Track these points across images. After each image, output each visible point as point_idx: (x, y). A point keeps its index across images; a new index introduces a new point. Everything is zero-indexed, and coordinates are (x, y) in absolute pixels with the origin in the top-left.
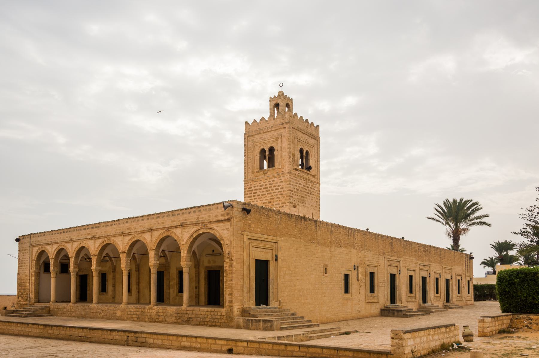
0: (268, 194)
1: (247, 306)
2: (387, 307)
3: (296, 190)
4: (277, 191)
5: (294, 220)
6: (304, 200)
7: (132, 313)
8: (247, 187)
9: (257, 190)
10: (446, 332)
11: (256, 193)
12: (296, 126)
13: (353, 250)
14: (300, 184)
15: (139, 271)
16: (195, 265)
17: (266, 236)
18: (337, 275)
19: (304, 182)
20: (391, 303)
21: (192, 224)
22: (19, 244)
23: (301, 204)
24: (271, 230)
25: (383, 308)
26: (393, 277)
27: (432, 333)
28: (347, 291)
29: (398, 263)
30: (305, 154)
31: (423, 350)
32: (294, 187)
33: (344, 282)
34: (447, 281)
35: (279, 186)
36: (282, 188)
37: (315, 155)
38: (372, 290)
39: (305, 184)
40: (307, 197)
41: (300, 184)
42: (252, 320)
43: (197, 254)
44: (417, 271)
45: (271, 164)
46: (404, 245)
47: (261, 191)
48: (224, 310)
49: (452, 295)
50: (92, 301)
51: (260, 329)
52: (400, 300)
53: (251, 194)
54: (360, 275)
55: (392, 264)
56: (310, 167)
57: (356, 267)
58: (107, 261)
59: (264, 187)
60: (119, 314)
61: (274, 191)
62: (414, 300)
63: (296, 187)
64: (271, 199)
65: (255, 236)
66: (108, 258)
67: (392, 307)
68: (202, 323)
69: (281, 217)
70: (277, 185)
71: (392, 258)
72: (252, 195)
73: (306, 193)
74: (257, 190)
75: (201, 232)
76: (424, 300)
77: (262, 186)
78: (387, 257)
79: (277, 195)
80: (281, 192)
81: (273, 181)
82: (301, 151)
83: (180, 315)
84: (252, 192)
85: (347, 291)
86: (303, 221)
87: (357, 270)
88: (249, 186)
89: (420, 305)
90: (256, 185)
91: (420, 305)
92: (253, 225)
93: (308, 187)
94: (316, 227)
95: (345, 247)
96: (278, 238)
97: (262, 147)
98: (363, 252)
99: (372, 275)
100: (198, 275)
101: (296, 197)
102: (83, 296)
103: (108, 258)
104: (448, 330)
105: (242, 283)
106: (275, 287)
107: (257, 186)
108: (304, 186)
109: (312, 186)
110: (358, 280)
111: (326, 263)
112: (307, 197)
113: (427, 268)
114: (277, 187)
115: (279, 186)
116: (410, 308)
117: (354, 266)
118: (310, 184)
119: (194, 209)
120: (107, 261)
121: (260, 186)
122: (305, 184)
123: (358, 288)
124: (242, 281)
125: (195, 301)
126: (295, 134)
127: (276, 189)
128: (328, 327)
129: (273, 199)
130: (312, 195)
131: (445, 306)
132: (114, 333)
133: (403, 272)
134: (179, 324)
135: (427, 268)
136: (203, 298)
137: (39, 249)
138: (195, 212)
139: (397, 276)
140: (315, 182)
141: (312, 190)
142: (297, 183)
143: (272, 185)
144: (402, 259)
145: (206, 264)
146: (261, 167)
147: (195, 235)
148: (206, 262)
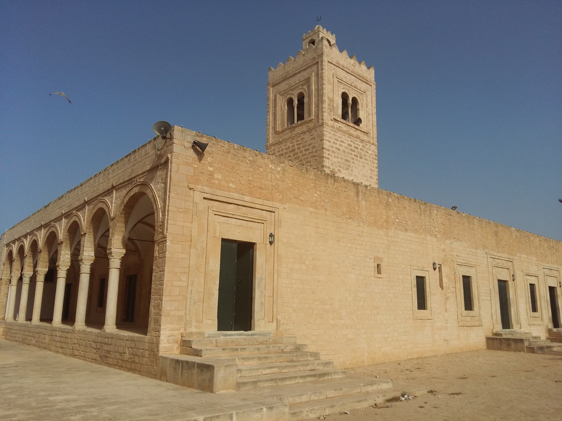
1: (193, 330)
2: (496, 334)
4: (307, 152)
6: (349, 166)
12: (335, 60)
13: (429, 238)
14: (342, 142)
17: (247, 198)
18: (401, 277)
19: (349, 139)
20: (504, 328)
24: (261, 188)
25: (490, 335)
26: (503, 286)
28: (422, 304)
29: (510, 264)
32: (331, 144)
33: (415, 289)
35: (309, 145)
36: (315, 147)
37: (367, 105)
38: (469, 305)
39: (352, 143)
41: (342, 142)
46: (516, 236)
47: (287, 156)
48: (147, 338)
52: (519, 322)
54: (444, 280)
55: (500, 265)
57: (437, 266)
59: (291, 149)
61: (304, 153)
62: (539, 322)
65: (221, 194)
67: (506, 334)
69: (284, 170)
70: (307, 144)
71: (499, 254)
73: (353, 156)
77: (289, 148)
78: (492, 253)
79: (307, 158)
80: (312, 152)
81: (302, 139)
82: (345, 96)
85: (422, 304)
86: (330, 181)
87: (440, 271)
90: (281, 149)
92: (217, 176)
93: (356, 148)
95: (416, 231)
96: (277, 205)
97: (288, 97)
98: (448, 242)
99: (467, 280)
101: (336, 160)
105: (185, 284)
107: (282, 150)
108: (349, 145)
109: (363, 146)
110: (441, 286)
111: (379, 256)
112: (355, 161)
113: (555, 273)
114: (307, 147)
115: (309, 145)
116: (535, 334)
117: (434, 264)
121: (286, 149)
122: (352, 143)
123: (445, 300)
126: (333, 72)
127: (305, 150)
130: (363, 160)
133: (518, 279)
137: (48, 230)
139: (510, 283)
140: (369, 142)
141: (363, 153)
142: (337, 140)
144: (515, 258)
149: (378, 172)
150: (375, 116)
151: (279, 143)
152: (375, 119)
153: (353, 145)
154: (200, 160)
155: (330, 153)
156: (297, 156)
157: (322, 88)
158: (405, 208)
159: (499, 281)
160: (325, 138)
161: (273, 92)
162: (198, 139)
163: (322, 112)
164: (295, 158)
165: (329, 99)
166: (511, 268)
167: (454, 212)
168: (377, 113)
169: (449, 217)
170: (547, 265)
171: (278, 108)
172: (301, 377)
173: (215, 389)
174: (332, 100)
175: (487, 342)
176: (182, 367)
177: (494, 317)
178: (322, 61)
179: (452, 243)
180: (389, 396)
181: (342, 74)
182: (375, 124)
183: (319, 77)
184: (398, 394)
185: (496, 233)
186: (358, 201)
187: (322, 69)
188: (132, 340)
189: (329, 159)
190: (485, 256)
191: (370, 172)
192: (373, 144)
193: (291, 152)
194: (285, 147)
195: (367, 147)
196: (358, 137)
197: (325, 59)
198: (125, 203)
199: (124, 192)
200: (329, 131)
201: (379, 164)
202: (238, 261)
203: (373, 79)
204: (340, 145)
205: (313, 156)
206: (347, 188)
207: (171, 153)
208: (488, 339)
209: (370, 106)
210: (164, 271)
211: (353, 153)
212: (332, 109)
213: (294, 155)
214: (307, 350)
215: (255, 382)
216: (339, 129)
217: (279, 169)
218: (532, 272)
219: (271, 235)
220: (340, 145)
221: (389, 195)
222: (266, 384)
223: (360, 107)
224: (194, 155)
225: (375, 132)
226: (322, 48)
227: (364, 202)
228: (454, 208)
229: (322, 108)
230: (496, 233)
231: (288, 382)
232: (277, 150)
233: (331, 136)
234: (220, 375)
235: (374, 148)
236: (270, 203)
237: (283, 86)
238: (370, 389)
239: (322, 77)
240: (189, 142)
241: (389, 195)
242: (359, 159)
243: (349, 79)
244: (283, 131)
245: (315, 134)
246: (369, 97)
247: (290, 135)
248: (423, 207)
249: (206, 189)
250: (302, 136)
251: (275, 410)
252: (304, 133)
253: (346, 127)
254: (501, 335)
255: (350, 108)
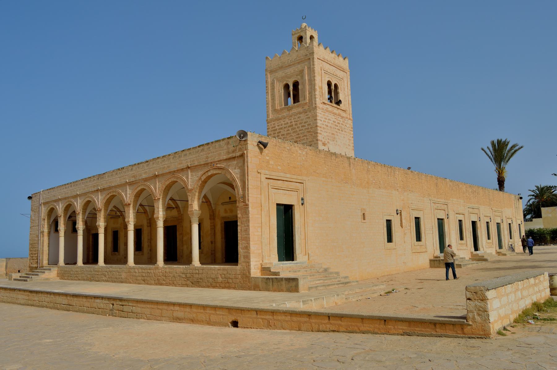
0: (294, 132)
2: (436, 257)
3: (325, 127)
4: (304, 128)
5: (323, 156)
6: (334, 138)
7: (137, 275)
8: (270, 127)
9: (281, 128)
10: (535, 285)
11: (280, 132)
14: (329, 120)
15: (150, 226)
16: (210, 215)
17: (288, 176)
19: (334, 117)
20: (441, 253)
21: (201, 165)
22: (32, 202)
23: (331, 142)
25: (432, 258)
26: (441, 222)
27: (520, 287)
28: (390, 240)
29: (446, 206)
30: (333, 87)
31: (512, 314)
34: (498, 225)
35: (305, 123)
36: (309, 124)
38: (419, 238)
40: (338, 134)
41: (329, 120)
42: (272, 279)
43: (212, 203)
44: (466, 215)
45: (296, 99)
47: (286, 129)
48: (238, 267)
49: (504, 241)
50: (189, 261)
51: (282, 291)
53: (274, 134)
54: (403, 221)
56: (340, 101)
57: (399, 212)
58: (119, 217)
59: (289, 124)
60: (124, 275)
61: (301, 128)
62: (465, 248)
63: (324, 123)
64: (297, 138)
65: (274, 175)
66: (118, 213)
68: (214, 284)
69: (307, 153)
71: (438, 200)
72: (276, 135)
74: (281, 128)
75: (210, 174)
76: (476, 248)
77: (287, 123)
79: (303, 133)
80: (308, 129)
81: (299, 117)
82: (329, 84)
83: (188, 275)
84: (276, 132)
85: (390, 240)
86: (334, 157)
87: (401, 215)
88: (273, 126)
89: (472, 253)
91: (472, 253)
92: (271, 162)
93: (339, 123)
94: (350, 164)
97: (285, 82)
100: (213, 227)
101: (325, 134)
102: (91, 257)
103: (118, 213)
104: (537, 281)
106: (303, 237)
107: (281, 125)
108: (334, 121)
109: (343, 122)
110: (402, 226)
112: (338, 134)
113: (476, 211)
114: (303, 124)
115: (305, 123)
117: (397, 210)
118: (341, 120)
119: (201, 148)
120: (119, 217)
121: (285, 124)
123: (404, 233)
124: (260, 230)
125: (208, 257)
127: (302, 126)
128: (542, 251)
129: (300, 137)
130: (343, 132)
131: (498, 253)
132: (98, 301)
133: (451, 216)
134: (187, 286)
135: (476, 211)
136: (220, 255)
138: (203, 150)
139: (446, 220)
140: (347, 118)
141: (343, 127)
142: (326, 119)
143: (298, 123)
144: (449, 202)
145: (223, 214)
146: (286, 103)
147: (203, 178)
148: (222, 212)
149: (354, 140)
150: (350, 97)
151: (278, 119)
152: (350, 99)
153: (336, 121)
154: (261, 153)
155: (322, 129)
156: (295, 130)
157: (315, 80)
158: (378, 172)
159: (438, 219)
160: (318, 118)
161: (270, 77)
162: (260, 139)
163: (315, 98)
164: (294, 132)
165: (319, 87)
166: (446, 210)
167: (409, 171)
168: (351, 94)
169: (406, 175)
170: (471, 206)
171: (276, 91)
172: (337, 284)
173: (300, 291)
174: (321, 88)
175: (430, 263)
176: (272, 282)
177: (435, 245)
178: (313, 58)
179: (408, 195)
180: (387, 291)
181: (327, 67)
182: (350, 103)
183: (311, 70)
184: (391, 290)
185: (437, 185)
186: (350, 170)
187: (314, 65)
188: (224, 270)
189: (321, 134)
190: (429, 202)
191: (348, 141)
192: (350, 119)
193: (289, 127)
194: (283, 123)
195: (346, 122)
196: (339, 115)
197: (316, 56)
198: (203, 179)
199: (200, 173)
200: (320, 112)
201: (354, 134)
202: (286, 213)
203: (348, 68)
204: (328, 122)
205: (309, 132)
206: (343, 161)
207: (246, 150)
208: (431, 261)
209: (346, 90)
210: (248, 226)
211: (337, 128)
212: (322, 95)
213: (292, 129)
214: (331, 271)
215: (317, 287)
216: (327, 111)
217: (304, 153)
218: (461, 212)
219: (302, 199)
220: (328, 122)
221: (368, 163)
222: (321, 288)
223: (339, 90)
224: (258, 150)
225: (351, 109)
226: (313, 48)
227: (354, 170)
228: (409, 168)
229: (315, 95)
230: (437, 185)
231: (331, 287)
232: (276, 125)
233: (322, 116)
234: (301, 283)
235: (350, 122)
236: (300, 177)
237: (280, 74)
238: (375, 288)
239: (314, 70)
240: (256, 142)
241: (368, 163)
242: (340, 132)
243: (332, 69)
244: (282, 109)
245: (310, 114)
246: (346, 82)
247: (288, 113)
248: (389, 170)
249: (267, 172)
250: (299, 115)
251: (339, 296)
252: (300, 113)
253: (332, 107)
254: (439, 257)
255: (333, 91)
